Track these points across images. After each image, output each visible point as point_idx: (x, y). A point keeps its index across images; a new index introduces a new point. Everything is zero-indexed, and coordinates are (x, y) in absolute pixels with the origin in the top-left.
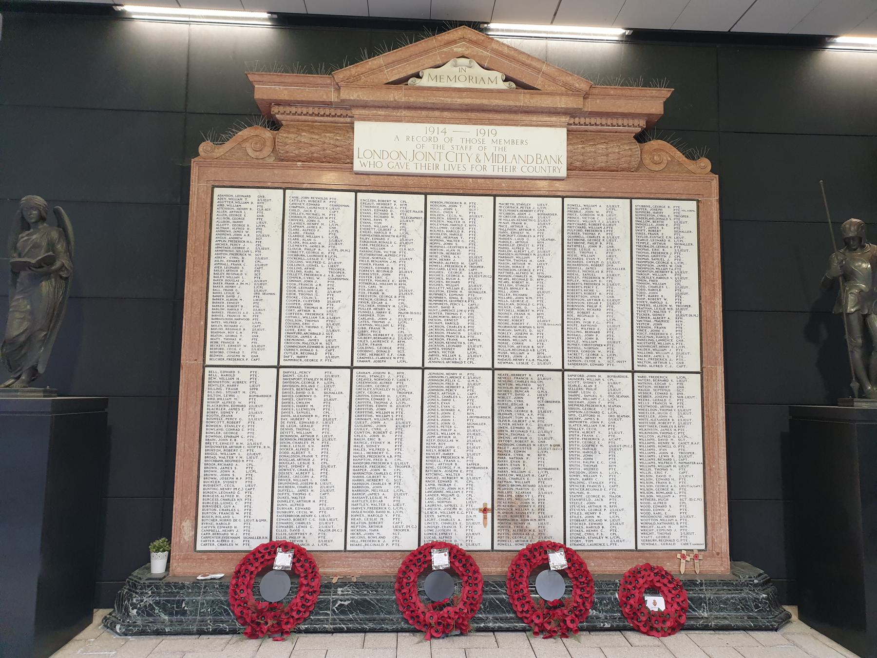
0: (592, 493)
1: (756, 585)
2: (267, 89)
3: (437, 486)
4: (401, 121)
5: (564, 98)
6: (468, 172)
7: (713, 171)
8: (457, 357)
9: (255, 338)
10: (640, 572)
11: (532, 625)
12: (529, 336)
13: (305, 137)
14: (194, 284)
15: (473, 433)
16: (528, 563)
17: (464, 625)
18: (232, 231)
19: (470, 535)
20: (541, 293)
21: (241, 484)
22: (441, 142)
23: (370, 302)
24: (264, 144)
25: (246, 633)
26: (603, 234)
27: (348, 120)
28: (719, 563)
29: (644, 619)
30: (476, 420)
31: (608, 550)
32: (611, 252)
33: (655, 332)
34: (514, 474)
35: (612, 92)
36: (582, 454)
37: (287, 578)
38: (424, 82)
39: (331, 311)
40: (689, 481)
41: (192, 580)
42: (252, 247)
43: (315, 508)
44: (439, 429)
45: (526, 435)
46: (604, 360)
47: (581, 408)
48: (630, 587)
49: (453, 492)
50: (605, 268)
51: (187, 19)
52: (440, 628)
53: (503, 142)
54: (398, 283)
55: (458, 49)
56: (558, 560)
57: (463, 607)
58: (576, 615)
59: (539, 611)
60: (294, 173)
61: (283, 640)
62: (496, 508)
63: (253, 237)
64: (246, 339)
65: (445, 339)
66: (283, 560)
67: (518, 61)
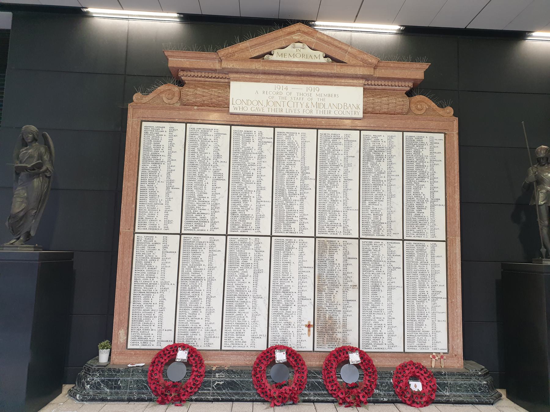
0: (377, 316)
1: (480, 376)
2: (176, 61)
3: (279, 310)
4: (259, 82)
5: (361, 69)
6: (301, 114)
7: (454, 115)
8: (293, 230)
9: (166, 216)
11: (338, 399)
12: (338, 217)
13: (199, 91)
15: (302, 277)
17: (295, 398)
19: (299, 342)
21: (156, 307)
22: (284, 95)
23: (239, 194)
24: (174, 95)
25: (158, 401)
26: (385, 154)
27: (227, 80)
28: (456, 361)
29: (409, 396)
30: (304, 269)
31: (388, 352)
33: (418, 215)
34: (328, 304)
37: (184, 367)
38: (274, 57)
39: (214, 200)
40: (438, 310)
41: (125, 367)
42: (165, 159)
43: (202, 323)
44: (281, 274)
45: (335, 279)
46: (385, 233)
47: (370, 262)
48: (400, 375)
50: (386, 175)
51: (127, 17)
52: (280, 399)
55: (296, 37)
56: (354, 358)
57: (294, 387)
58: (366, 393)
59: (342, 390)
61: (181, 405)
63: (166, 153)
64: (161, 216)
65: (285, 218)
66: (182, 355)
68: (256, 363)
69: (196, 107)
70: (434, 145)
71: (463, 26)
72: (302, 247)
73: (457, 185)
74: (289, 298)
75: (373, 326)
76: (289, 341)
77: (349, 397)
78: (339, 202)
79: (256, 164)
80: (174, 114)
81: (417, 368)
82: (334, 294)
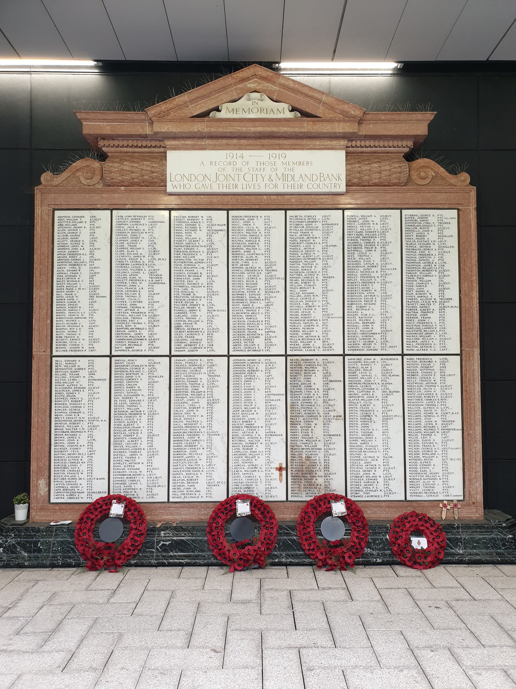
0: (369, 454)
1: (504, 528)
2: (92, 126)
3: (241, 450)
4: (205, 149)
5: (341, 124)
6: (263, 190)
7: (471, 183)
8: (257, 346)
9: (91, 333)
10: (407, 518)
11: (317, 560)
12: (316, 328)
13: (127, 166)
14: (41, 290)
15: (270, 408)
16: (314, 511)
17: (261, 560)
18: (70, 246)
19: (269, 489)
20: (326, 291)
21: (84, 450)
23: (184, 302)
24: (94, 173)
25: (87, 567)
26: (377, 240)
27: (162, 150)
28: (474, 510)
29: (409, 555)
30: (272, 397)
31: (382, 501)
32: (384, 254)
33: (422, 321)
34: (304, 440)
35: (383, 117)
36: (360, 423)
37: (120, 524)
38: (223, 114)
39: (152, 310)
40: (450, 444)
41: (46, 525)
42: (87, 259)
43: (143, 468)
44: (243, 405)
45: (313, 408)
46: (378, 346)
47: (359, 385)
48: (398, 530)
49: (255, 455)
51: (29, 70)
52: (242, 562)
53: (291, 163)
54: (206, 285)
55: (251, 85)
56: (339, 508)
57: (261, 546)
58: (353, 553)
59: (323, 550)
60: (117, 197)
61: (116, 571)
62: (289, 467)
63: (87, 251)
65: (246, 331)
66: (117, 509)
67: (302, 93)
68: (212, 518)
69: (123, 188)
70: (444, 225)
71: (483, 58)
72: (269, 368)
73: (475, 278)
74: (254, 435)
75: (364, 468)
76: (255, 489)
77: (331, 558)
78: (317, 307)
79: (205, 260)
80: (95, 198)
81: (421, 520)
82: (313, 427)
